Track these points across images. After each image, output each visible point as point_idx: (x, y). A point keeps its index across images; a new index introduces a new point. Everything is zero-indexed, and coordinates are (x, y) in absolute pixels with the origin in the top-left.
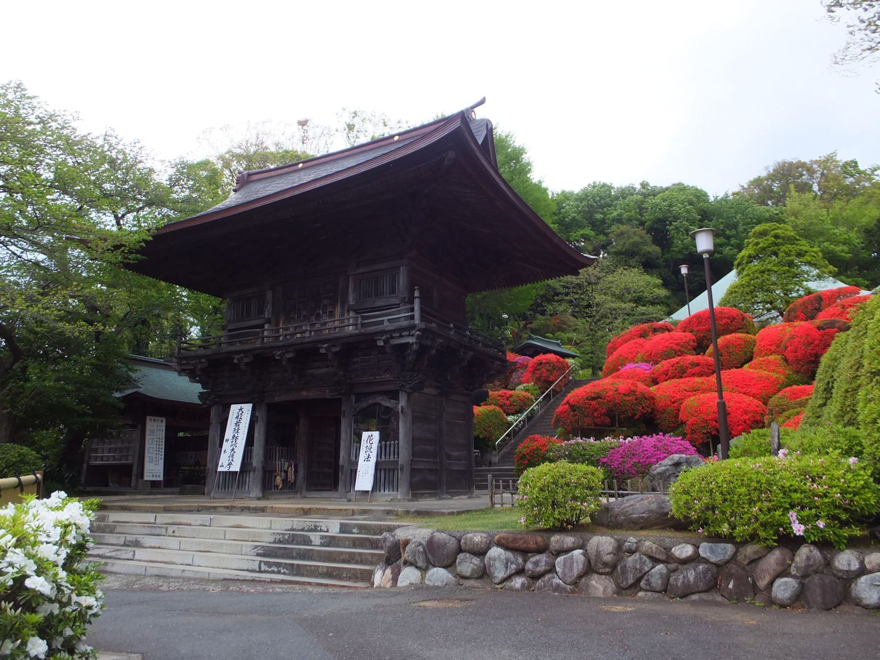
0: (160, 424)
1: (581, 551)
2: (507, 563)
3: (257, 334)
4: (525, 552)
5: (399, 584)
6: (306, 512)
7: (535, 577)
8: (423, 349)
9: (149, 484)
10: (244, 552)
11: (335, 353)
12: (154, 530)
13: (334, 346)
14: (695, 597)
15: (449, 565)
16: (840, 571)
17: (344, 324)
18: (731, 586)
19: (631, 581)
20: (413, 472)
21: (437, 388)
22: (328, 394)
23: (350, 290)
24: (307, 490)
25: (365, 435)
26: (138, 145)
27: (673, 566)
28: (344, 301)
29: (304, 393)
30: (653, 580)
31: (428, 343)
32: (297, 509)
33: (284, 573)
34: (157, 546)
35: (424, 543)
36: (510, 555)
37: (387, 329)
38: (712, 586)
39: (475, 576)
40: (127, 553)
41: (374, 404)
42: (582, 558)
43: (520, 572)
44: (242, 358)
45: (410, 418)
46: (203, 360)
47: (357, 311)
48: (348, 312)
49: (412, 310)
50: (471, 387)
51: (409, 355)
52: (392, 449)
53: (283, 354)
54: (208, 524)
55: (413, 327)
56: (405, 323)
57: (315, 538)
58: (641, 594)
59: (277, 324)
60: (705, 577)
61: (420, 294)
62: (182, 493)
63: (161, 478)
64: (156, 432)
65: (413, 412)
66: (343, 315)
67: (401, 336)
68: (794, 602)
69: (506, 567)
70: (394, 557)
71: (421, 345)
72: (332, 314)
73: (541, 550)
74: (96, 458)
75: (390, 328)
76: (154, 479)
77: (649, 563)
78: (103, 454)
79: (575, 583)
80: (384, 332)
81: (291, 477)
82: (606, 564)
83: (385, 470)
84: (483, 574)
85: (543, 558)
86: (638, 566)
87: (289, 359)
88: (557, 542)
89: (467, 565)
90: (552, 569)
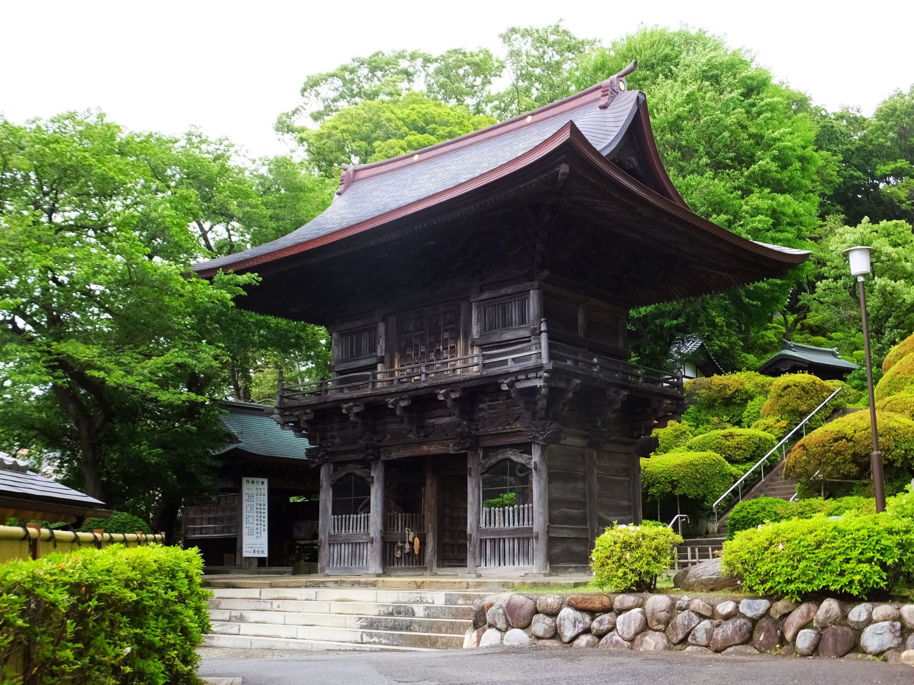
0: (260, 486)
1: (640, 609)
2: (575, 622)
3: (366, 378)
4: (593, 613)
5: (481, 645)
6: (419, 586)
7: (600, 636)
8: (554, 393)
9: (256, 563)
10: (347, 625)
11: (455, 400)
12: (260, 606)
13: (453, 391)
14: (730, 649)
15: (526, 627)
16: (852, 622)
17: (465, 363)
18: (761, 639)
19: (681, 637)
20: (551, 541)
21: (585, 437)
22: (451, 449)
23: (474, 320)
24: (438, 566)
26: (226, 143)
27: (716, 622)
28: (467, 333)
29: (425, 448)
30: (697, 635)
31: (562, 385)
32: (410, 583)
33: (385, 644)
34: (262, 620)
35: (504, 605)
36: (578, 614)
37: (511, 370)
38: (748, 640)
39: (548, 635)
40: (233, 628)
42: (640, 615)
43: (587, 631)
44: (351, 408)
45: (544, 475)
46: (308, 411)
47: (482, 347)
48: (472, 347)
50: (635, 433)
51: (539, 400)
53: (397, 402)
54: (314, 598)
56: (531, 363)
57: (419, 610)
58: (689, 648)
59: (392, 366)
60: (740, 630)
61: (547, 326)
62: (295, 573)
63: (266, 555)
64: (255, 499)
65: (549, 468)
66: (466, 352)
67: (528, 379)
68: (813, 652)
69: (575, 627)
70: (480, 621)
71: (551, 389)
72: (453, 350)
73: (608, 610)
74: (194, 531)
75: (514, 370)
77: (696, 619)
79: (632, 641)
80: (507, 374)
82: (659, 622)
84: (556, 635)
85: (607, 617)
86: (686, 623)
87: (404, 408)
88: (620, 601)
89: (541, 625)
90: (613, 628)
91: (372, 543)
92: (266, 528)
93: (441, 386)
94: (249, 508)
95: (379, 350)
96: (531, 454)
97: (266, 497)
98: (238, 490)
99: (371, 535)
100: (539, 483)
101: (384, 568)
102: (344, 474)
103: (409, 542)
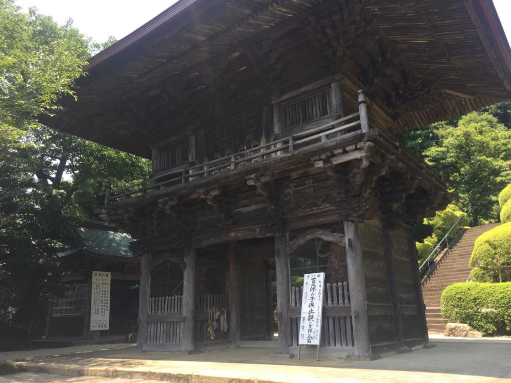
13: (263, 175)
20: (371, 319)
22: (258, 234)
23: (275, 119)
24: (241, 339)
25: (308, 279)
29: (233, 234)
31: (378, 160)
41: (313, 240)
44: (166, 202)
45: (359, 252)
49: (358, 118)
52: (340, 292)
55: (360, 138)
63: (107, 328)
64: (101, 285)
76: (102, 329)
78: (61, 309)
80: (323, 150)
81: (224, 325)
83: (334, 318)
91: (184, 321)
92: (109, 308)
93: (248, 172)
94: (96, 294)
95: (190, 158)
96: (343, 232)
97: (109, 286)
98: (88, 280)
99: (184, 314)
100: (355, 259)
101: (195, 346)
102: (160, 262)
103: (216, 320)
